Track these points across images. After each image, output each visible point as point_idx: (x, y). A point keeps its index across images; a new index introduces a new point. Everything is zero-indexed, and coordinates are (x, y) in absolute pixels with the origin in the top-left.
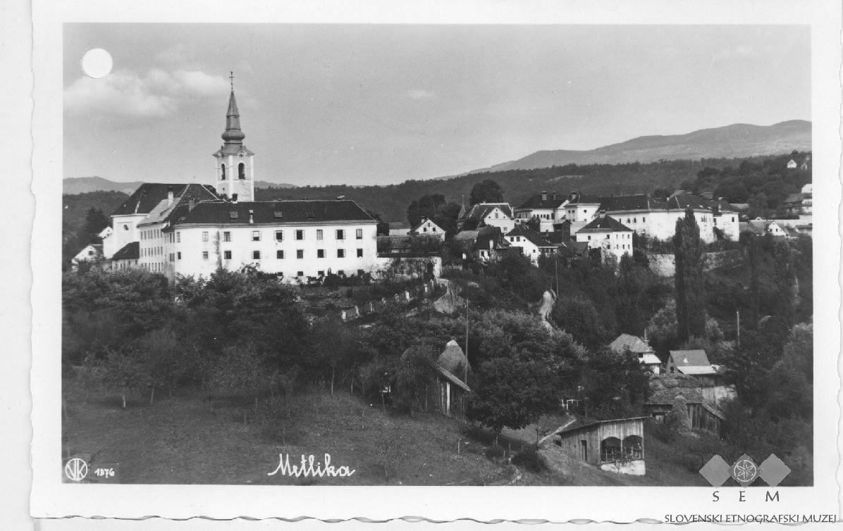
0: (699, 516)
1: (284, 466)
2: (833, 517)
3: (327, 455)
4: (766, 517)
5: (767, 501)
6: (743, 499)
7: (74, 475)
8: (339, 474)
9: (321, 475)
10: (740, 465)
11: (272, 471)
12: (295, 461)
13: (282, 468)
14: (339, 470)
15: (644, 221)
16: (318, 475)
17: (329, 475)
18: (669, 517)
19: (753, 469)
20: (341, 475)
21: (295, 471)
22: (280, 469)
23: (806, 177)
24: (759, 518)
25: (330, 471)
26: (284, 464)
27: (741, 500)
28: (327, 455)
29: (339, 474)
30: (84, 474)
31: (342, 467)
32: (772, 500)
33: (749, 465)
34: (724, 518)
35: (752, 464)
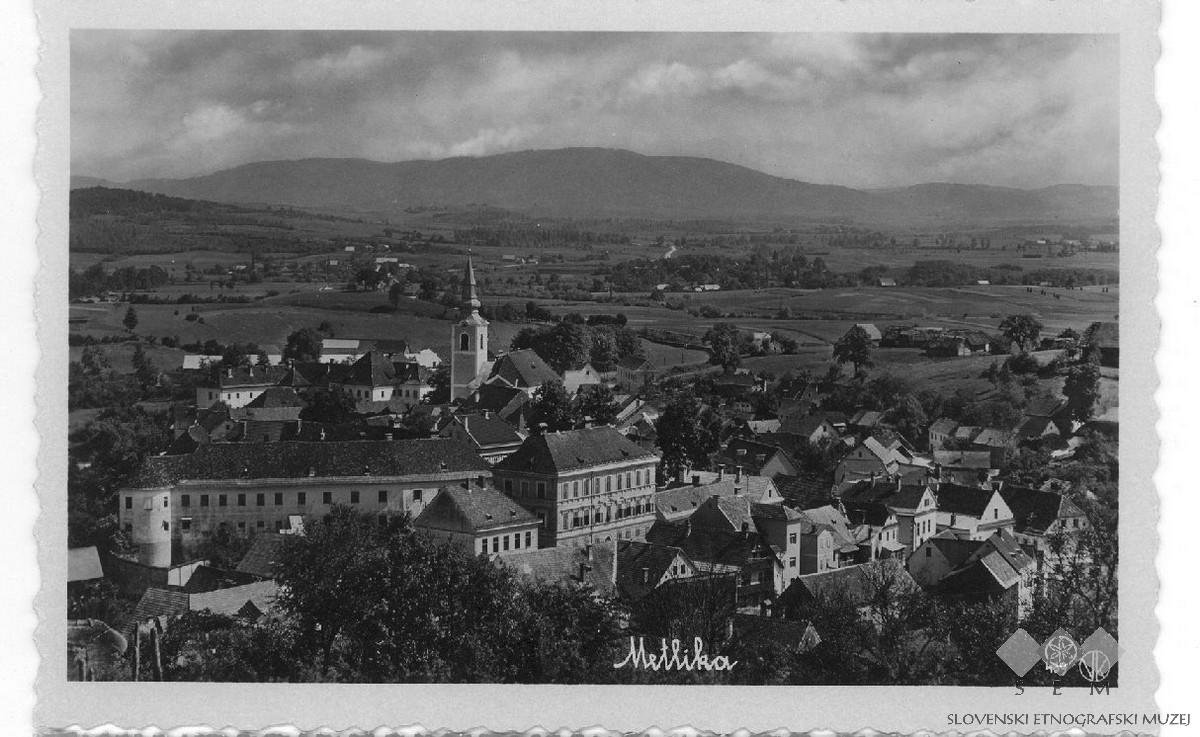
0: (996, 716)
2: (1186, 717)
3: (697, 639)
4: (1091, 717)
9: (689, 668)
10: (1053, 643)
12: (653, 648)
14: (715, 662)
15: (238, 397)
17: (700, 668)
18: (953, 718)
19: (1072, 650)
21: (652, 662)
25: (701, 660)
27: (1055, 693)
31: (721, 657)
32: (1099, 693)
33: (1067, 643)
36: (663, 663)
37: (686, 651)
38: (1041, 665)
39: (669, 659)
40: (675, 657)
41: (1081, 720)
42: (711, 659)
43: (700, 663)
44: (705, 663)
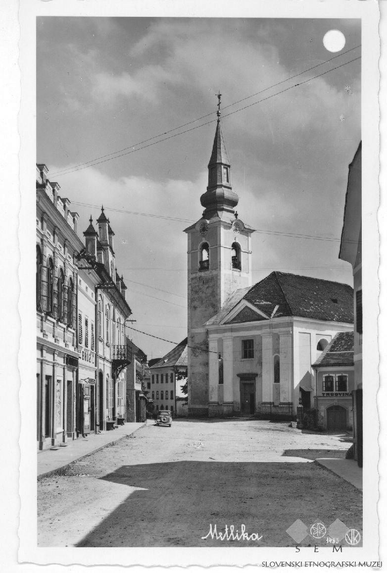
1: (212, 532)
3: (243, 525)
5: (333, 552)
6: (317, 550)
7: (351, 541)
8: (251, 539)
10: (314, 526)
11: (205, 536)
13: (212, 535)
14: (251, 536)
16: (236, 539)
18: (265, 563)
19: (355, 532)
20: (253, 539)
22: (210, 534)
23: (122, 425)
24: (369, 564)
25: (245, 535)
26: (213, 532)
27: (315, 551)
28: (243, 525)
29: (251, 539)
30: (358, 540)
32: (337, 551)
33: (321, 526)
34: (304, 563)
35: (323, 526)
36: (226, 538)
37: (237, 531)
38: (309, 537)
39: (229, 535)
40: (232, 534)
41: (328, 564)
42: (249, 535)
43: (244, 536)
44: (247, 537)
